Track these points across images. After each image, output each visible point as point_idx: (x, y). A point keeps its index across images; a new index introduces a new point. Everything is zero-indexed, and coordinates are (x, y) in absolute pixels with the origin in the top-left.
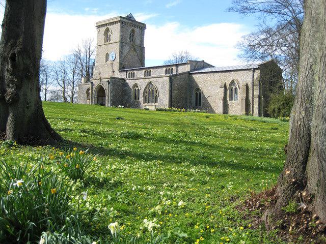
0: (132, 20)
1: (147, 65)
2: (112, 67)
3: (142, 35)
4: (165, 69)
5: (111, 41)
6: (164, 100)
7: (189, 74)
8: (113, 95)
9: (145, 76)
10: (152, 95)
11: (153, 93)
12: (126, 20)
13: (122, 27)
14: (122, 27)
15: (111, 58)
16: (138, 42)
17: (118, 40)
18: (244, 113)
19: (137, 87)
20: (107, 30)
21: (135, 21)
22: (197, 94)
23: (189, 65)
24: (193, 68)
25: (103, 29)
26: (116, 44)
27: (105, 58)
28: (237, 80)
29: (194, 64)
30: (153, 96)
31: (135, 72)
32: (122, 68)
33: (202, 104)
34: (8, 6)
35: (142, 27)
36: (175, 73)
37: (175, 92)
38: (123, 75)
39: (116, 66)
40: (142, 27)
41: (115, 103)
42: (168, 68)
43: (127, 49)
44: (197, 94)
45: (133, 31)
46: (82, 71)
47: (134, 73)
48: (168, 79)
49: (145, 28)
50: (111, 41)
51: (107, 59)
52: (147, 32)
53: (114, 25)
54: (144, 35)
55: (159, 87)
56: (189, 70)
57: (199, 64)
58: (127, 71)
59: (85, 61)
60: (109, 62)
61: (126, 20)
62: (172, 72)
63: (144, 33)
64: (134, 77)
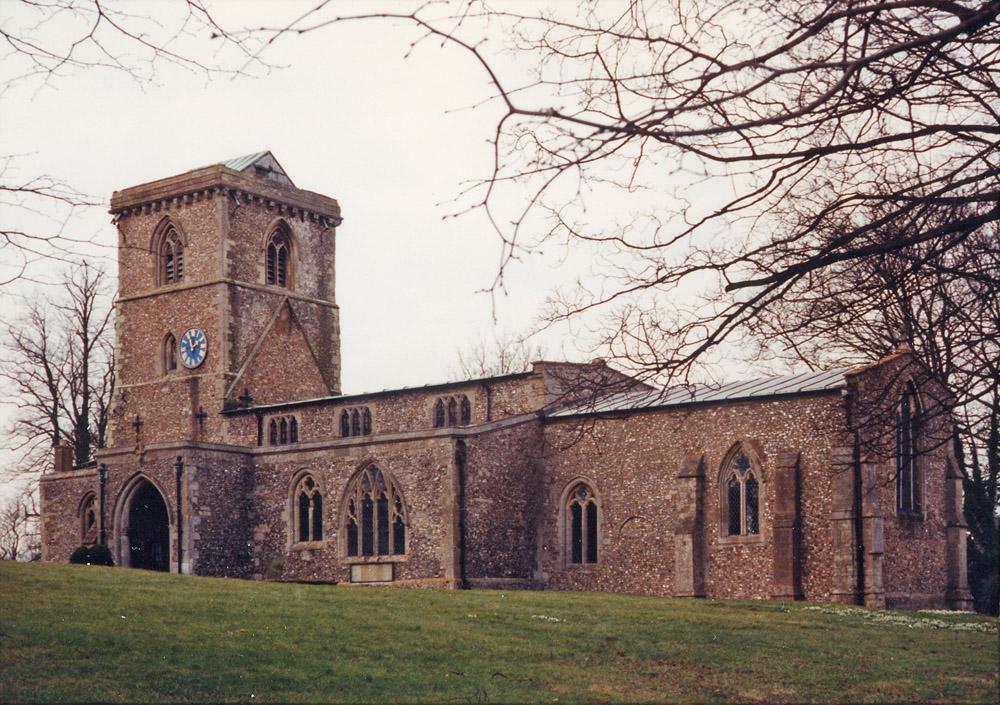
1: (354, 380)
2: (194, 394)
3: (325, 249)
4: (431, 401)
6: (432, 533)
8: (204, 520)
9: (345, 433)
10: (378, 529)
11: (383, 511)
14: (232, 216)
18: (790, 589)
20: (167, 229)
21: (290, 187)
22: (576, 508)
25: (145, 225)
26: (512, 235)
28: (755, 443)
32: (231, 370)
33: (600, 553)
34: (335, 324)
37: (480, 507)
42: (449, 402)
44: (576, 508)
45: (284, 233)
46: (54, 417)
48: (450, 446)
52: (344, 236)
53: (195, 207)
54: (332, 253)
55: (409, 480)
59: (67, 369)
62: (466, 418)
63: (333, 245)
64: (294, 439)
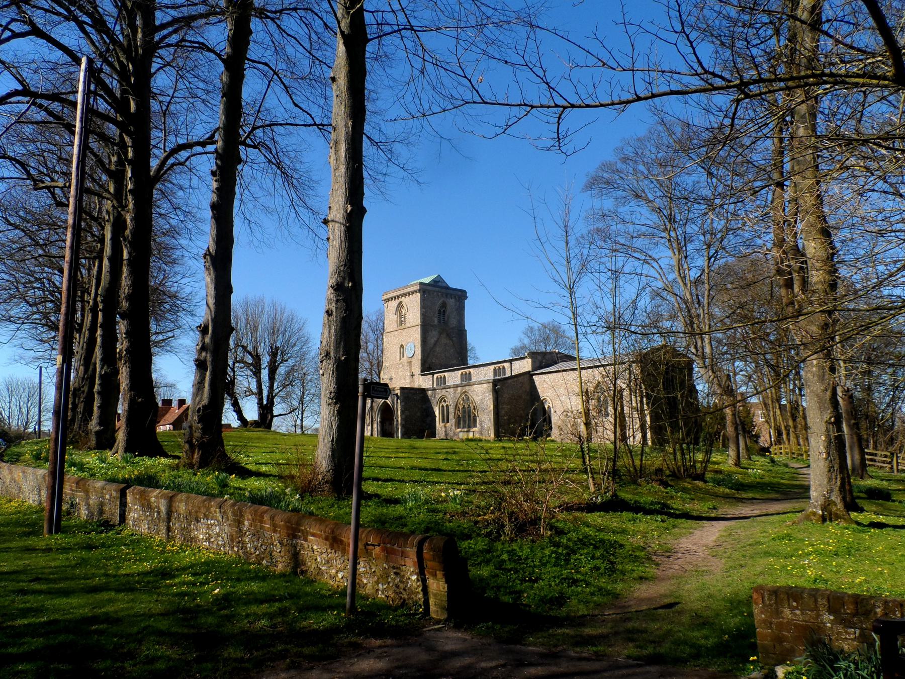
0: (441, 287)
2: (410, 367)
3: (461, 310)
5: (408, 325)
7: (529, 375)
10: (467, 418)
12: (429, 288)
13: (423, 301)
15: (408, 354)
16: (453, 322)
17: (418, 322)
19: (445, 401)
21: (448, 288)
23: (530, 360)
24: (538, 365)
26: (412, 324)
27: (398, 354)
29: (540, 358)
30: (469, 416)
31: (446, 374)
32: (427, 367)
35: (460, 296)
36: (508, 374)
37: (505, 408)
38: (424, 382)
39: (417, 368)
40: (460, 296)
41: (406, 435)
43: (433, 336)
45: (444, 305)
47: (470, 373)
49: (466, 297)
50: (408, 325)
51: (402, 355)
56: (530, 369)
57: (548, 357)
58: (433, 374)
60: (405, 359)
61: (429, 288)
